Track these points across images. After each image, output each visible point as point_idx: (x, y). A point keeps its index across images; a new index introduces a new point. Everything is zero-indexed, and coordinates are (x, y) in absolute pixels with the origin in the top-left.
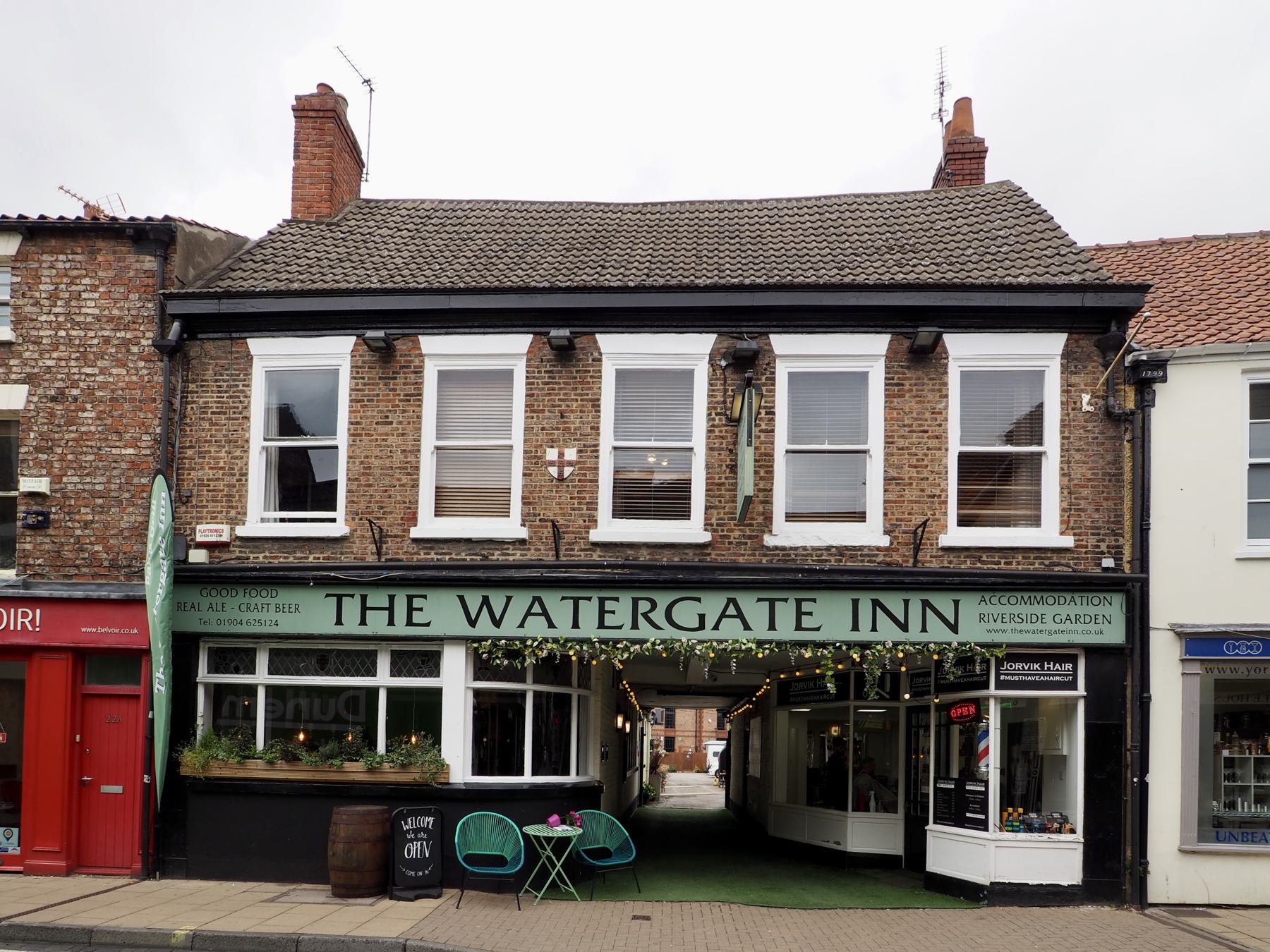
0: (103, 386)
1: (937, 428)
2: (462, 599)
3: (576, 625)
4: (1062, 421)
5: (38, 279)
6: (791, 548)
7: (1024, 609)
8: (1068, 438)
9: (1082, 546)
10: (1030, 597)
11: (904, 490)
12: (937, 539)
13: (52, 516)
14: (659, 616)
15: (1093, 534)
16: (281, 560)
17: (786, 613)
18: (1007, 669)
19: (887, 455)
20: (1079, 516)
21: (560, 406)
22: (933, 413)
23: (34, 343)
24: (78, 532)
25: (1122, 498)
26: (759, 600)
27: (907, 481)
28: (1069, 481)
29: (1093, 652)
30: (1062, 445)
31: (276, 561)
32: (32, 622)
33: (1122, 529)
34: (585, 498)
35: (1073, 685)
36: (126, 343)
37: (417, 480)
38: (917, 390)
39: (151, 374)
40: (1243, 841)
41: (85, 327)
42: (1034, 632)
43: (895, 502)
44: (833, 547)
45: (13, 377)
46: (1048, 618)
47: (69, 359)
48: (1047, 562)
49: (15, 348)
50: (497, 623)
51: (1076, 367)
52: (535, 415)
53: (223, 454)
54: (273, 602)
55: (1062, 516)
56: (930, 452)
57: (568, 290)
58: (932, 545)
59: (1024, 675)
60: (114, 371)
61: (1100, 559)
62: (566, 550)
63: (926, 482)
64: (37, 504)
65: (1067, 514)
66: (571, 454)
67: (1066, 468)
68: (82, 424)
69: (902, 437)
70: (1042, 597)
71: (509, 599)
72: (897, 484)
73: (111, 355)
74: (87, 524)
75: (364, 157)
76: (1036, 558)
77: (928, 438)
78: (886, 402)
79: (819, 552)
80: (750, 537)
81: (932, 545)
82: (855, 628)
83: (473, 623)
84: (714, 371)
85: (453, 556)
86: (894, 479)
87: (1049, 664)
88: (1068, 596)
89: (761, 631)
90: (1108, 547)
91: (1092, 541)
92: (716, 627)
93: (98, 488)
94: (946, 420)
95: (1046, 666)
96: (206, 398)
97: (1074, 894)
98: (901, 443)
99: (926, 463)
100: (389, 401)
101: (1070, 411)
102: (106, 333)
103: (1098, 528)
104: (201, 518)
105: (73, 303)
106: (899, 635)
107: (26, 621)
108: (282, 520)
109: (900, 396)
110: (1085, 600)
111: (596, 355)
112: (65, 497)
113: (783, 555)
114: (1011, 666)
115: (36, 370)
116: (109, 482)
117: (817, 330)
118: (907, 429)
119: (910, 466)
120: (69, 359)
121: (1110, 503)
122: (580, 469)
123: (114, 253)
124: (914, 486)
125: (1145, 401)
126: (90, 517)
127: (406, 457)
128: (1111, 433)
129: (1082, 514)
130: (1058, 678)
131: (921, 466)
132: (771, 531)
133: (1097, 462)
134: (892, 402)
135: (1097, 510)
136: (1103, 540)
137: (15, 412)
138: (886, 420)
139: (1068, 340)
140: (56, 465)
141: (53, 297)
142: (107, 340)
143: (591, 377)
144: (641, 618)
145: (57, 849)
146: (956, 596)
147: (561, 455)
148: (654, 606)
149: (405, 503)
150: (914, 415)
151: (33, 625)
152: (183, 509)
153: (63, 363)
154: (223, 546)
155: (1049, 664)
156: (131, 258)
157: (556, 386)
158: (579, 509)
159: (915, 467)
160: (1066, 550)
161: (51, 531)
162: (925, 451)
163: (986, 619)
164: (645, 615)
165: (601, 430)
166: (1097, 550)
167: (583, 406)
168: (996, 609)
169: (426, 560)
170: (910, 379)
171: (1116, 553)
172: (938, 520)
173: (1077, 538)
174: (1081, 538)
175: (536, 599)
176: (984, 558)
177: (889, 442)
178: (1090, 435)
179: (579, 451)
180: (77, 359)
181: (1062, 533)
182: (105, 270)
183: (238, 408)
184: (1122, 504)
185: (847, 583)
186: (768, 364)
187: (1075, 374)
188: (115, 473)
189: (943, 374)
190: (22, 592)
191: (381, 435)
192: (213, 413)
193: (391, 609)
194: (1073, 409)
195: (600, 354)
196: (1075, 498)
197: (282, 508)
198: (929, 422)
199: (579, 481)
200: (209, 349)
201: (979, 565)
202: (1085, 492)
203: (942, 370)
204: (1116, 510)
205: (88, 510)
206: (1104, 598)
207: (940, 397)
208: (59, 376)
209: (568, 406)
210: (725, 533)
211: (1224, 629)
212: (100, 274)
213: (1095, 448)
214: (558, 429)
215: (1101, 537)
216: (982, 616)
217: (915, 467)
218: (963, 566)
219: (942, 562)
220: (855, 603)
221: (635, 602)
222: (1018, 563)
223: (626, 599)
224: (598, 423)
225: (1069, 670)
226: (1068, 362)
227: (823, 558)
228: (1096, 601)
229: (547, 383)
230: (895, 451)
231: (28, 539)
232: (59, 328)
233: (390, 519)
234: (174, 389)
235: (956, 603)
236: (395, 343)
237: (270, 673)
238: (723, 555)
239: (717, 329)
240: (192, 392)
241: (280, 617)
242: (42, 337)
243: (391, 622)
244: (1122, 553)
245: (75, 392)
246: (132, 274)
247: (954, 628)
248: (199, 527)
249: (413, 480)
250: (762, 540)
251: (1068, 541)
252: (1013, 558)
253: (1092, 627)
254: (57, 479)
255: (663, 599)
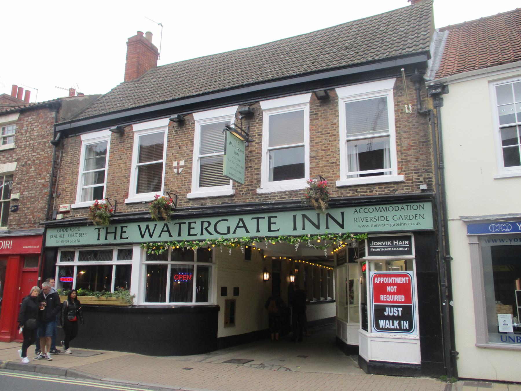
0: (38, 159)
1: (334, 131)
2: (139, 226)
3: (258, 231)
4: (396, 119)
5: (23, 126)
6: (269, 194)
7: (377, 214)
8: (399, 127)
9: (410, 180)
10: (380, 208)
11: (319, 161)
12: (335, 183)
13: (19, 207)
14: (211, 229)
15: (415, 173)
16: (85, 216)
17: (264, 224)
18: (374, 245)
19: (311, 146)
20: (407, 164)
21: (179, 144)
22: (332, 124)
23: (20, 147)
24: (26, 212)
25: (430, 154)
26: (253, 218)
27: (320, 157)
28: (401, 148)
29: (418, 234)
30: (396, 131)
31: (83, 216)
32: (10, 245)
33: (431, 169)
34: (187, 180)
35: (409, 252)
36: (45, 143)
37: (129, 180)
38: (324, 115)
39: (50, 151)
40: (517, 342)
41: (34, 139)
42: (376, 226)
43: (315, 167)
44: (287, 191)
45: (13, 160)
46: (390, 218)
47: (28, 152)
48: (391, 189)
49: (14, 150)
50: (151, 236)
51: (401, 93)
52: (170, 149)
53: (70, 178)
54: (78, 232)
55: (398, 165)
56: (331, 143)
57: (179, 99)
58: (333, 186)
59: (383, 248)
60: (41, 153)
61: (419, 185)
62: (179, 203)
63: (329, 157)
64: (16, 203)
65: (401, 164)
66: (182, 163)
67: (399, 142)
68: (30, 173)
69: (318, 137)
70: (386, 207)
71: (156, 225)
72: (316, 159)
73: (40, 148)
74: (28, 208)
75: (159, 52)
76: (385, 188)
77: (330, 136)
78: (310, 123)
79: (281, 194)
80: (251, 190)
81: (333, 186)
82: (295, 229)
83: (143, 236)
84: (237, 120)
85: (139, 209)
86: (314, 157)
87: (396, 241)
88: (400, 206)
89: (253, 233)
90: (424, 179)
91: (415, 176)
92: (234, 232)
93: (33, 195)
94: (338, 127)
95: (394, 242)
96: (67, 158)
97: (416, 370)
98: (317, 140)
99: (329, 148)
100: (122, 151)
101: (399, 114)
102: (40, 141)
103: (418, 170)
104: (62, 202)
105: (32, 132)
106: (315, 231)
107: (8, 245)
108: (362, 176)
109: (316, 119)
110: (409, 207)
111: (193, 121)
112: (23, 199)
113: (265, 197)
114: (376, 244)
115: (20, 157)
116: (36, 193)
117: (279, 96)
118: (320, 133)
119: (322, 150)
120: (28, 152)
121: (424, 156)
122: (185, 168)
123: (44, 113)
124: (324, 159)
125: (439, 104)
126: (29, 206)
127: (126, 172)
128: (422, 121)
129: (409, 163)
130: (401, 249)
131: (327, 150)
132: (260, 187)
133: (415, 137)
134: (313, 122)
135: (417, 161)
136: (421, 176)
137: (13, 171)
138: (310, 130)
139: (396, 81)
140: (22, 188)
141: (26, 131)
142: (40, 143)
143: (191, 131)
144: (204, 230)
145: (8, 332)
146: (342, 210)
147: (178, 164)
148: (209, 224)
149: (124, 189)
150: (323, 127)
151: (10, 247)
152: (58, 199)
153: (27, 153)
154: (67, 212)
155: (396, 241)
156: (49, 114)
157: (178, 136)
158: (185, 185)
159: (324, 150)
160: (401, 182)
161: (18, 212)
162: (329, 142)
163: (358, 220)
164: (206, 229)
165: (194, 152)
166: (418, 181)
167: (187, 143)
168: (363, 215)
169: (130, 212)
170: (321, 111)
171: (429, 181)
172: (336, 174)
173: (407, 175)
174: (409, 175)
175: (166, 225)
176: (359, 190)
177: (312, 140)
178: (411, 124)
179: (185, 161)
180: (31, 151)
181: (399, 174)
182: (41, 119)
183: (76, 160)
184: (430, 156)
185: (290, 208)
186: (259, 114)
187: (401, 96)
188: (38, 189)
189: (336, 106)
190: (7, 235)
191: (118, 164)
192: (69, 163)
193: (115, 233)
194: (401, 113)
195: (194, 121)
196: (405, 156)
197: (361, 169)
198: (330, 129)
199: (185, 173)
200: (70, 141)
201: (356, 194)
202: (410, 152)
203: (335, 105)
204: (427, 159)
205: (29, 203)
206: (420, 205)
207: (335, 117)
208: (26, 158)
209: (182, 143)
210: (241, 189)
211: (486, 218)
212: (40, 121)
213: (414, 130)
214: (178, 153)
215: (420, 174)
216: (356, 219)
217: (324, 150)
218: (348, 195)
219: (338, 194)
220: (295, 217)
221: (202, 223)
222: (376, 191)
223: (199, 221)
224: (193, 149)
225: (407, 244)
226: (397, 91)
227: (283, 197)
228: (415, 207)
229: (175, 136)
230: (315, 144)
231: (12, 215)
232: (27, 141)
233: (119, 196)
234: (58, 156)
235: (343, 213)
236: (124, 129)
237: (79, 260)
238: (240, 199)
239: (238, 103)
240: (64, 157)
241: (81, 238)
242: (22, 145)
243: (115, 238)
244: (431, 181)
245: (29, 162)
246: (48, 119)
247: (342, 226)
248: (61, 206)
249: (128, 180)
250: (256, 191)
251: (401, 178)
252: (374, 189)
253: (414, 221)
254: (22, 193)
255: (213, 221)
